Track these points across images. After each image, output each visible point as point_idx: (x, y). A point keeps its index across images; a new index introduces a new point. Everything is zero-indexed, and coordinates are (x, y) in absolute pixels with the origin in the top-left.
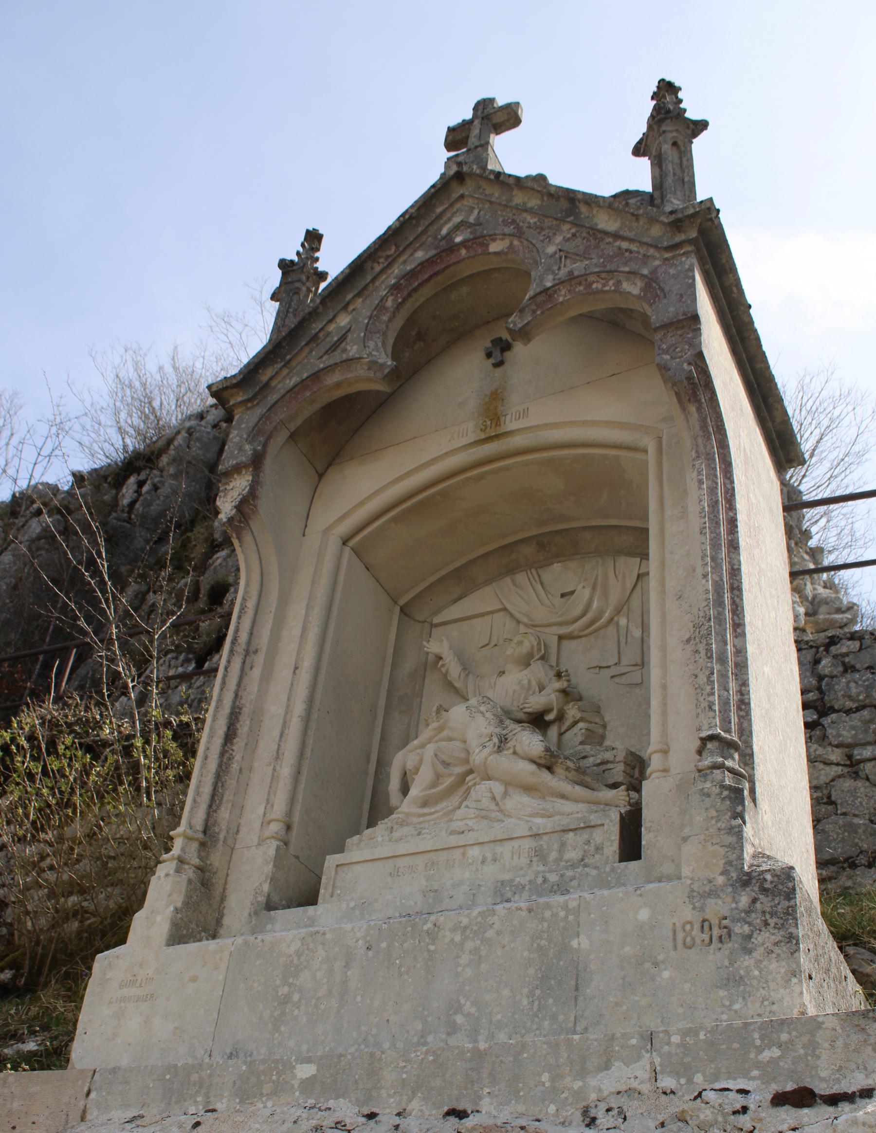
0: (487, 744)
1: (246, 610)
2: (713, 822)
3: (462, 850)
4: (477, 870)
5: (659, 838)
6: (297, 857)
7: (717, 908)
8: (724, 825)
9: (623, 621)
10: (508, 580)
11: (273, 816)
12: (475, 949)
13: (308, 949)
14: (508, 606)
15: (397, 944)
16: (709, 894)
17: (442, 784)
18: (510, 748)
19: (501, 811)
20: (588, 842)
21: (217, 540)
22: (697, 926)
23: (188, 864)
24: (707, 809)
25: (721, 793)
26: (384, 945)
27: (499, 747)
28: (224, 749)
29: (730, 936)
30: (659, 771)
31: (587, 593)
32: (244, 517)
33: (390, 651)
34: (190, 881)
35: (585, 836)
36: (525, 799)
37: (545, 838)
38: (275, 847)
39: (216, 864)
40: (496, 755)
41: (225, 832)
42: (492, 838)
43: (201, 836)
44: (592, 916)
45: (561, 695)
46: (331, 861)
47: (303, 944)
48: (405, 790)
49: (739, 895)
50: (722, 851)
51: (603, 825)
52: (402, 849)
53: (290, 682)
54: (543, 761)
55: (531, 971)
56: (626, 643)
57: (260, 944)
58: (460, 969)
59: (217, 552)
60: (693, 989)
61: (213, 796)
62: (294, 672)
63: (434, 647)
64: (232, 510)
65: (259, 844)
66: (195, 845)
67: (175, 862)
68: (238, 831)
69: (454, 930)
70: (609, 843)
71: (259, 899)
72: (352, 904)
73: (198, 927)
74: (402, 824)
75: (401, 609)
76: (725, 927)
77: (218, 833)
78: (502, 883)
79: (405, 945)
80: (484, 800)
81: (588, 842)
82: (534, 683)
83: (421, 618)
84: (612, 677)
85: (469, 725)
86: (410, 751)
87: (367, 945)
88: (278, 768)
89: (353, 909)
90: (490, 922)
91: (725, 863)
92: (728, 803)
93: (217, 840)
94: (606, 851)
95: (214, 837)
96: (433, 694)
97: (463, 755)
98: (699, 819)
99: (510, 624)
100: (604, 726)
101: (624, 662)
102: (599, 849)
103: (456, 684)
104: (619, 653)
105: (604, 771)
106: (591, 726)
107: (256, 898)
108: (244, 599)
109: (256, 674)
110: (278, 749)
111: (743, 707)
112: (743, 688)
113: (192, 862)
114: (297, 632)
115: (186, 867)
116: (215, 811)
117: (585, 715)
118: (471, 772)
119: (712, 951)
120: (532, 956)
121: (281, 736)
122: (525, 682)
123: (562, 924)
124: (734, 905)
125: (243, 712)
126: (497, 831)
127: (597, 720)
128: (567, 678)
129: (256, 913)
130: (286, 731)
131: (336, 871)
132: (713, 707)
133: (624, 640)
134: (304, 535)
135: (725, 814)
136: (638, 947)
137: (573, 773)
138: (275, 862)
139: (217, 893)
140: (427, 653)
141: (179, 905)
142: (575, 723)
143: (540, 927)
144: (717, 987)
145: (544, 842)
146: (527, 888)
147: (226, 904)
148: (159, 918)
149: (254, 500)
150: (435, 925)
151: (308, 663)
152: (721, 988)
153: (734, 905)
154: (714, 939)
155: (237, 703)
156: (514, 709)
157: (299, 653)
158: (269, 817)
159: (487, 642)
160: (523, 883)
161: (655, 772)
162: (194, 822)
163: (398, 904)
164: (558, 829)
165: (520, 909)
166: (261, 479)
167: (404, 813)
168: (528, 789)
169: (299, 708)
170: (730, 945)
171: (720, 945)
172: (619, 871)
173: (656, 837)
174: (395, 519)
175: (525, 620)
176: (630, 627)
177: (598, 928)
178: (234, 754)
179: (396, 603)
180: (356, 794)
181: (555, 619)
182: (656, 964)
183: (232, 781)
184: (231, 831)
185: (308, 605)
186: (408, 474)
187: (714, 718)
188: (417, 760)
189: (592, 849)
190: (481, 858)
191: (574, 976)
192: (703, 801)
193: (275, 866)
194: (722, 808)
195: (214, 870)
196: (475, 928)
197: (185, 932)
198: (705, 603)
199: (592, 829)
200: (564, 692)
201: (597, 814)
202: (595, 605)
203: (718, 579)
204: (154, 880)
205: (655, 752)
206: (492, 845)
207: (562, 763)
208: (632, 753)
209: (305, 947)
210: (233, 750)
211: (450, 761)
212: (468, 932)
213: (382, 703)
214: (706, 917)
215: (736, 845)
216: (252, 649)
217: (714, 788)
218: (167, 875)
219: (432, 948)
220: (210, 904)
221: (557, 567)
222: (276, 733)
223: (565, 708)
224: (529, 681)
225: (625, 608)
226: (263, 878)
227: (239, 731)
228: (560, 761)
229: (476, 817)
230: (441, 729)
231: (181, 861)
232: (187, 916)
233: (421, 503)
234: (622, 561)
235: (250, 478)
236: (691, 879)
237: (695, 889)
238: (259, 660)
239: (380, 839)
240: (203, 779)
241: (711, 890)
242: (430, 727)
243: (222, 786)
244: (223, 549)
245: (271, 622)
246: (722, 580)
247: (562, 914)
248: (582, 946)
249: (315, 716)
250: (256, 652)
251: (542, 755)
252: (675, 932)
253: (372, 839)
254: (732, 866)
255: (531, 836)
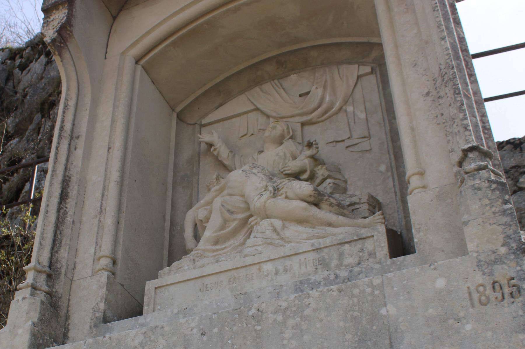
0: (264, 193)
1: (68, 107)
2: (488, 208)
3: (257, 266)
4: (272, 279)
5: (428, 236)
6: (122, 285)
7: (504, 272)
8: (497, 210)
9: (350, 109)
10: (257, 89)
11: (103, 254)
12: (297, 325)
13: (150, 341)
14: (259, 106)
15: (227, 329)
16: (495, 262)
17: (228, 227)
18: (282, 194)
19: (282, 239)
20: (362, 250)
21: (10, 132)
22: (489, 287)
23: (40, 290)
24: (480, 199)
25: (490, 186)
26: (216, 330)
27: (274, 194)
28: (60, 206)
29: (519, 292)
30: (419, 188)
31: (320, 92)
32: (63, 39)
33: (173, 144)
34: (42, 303)
35: (359, 245)
36: (300, 228)
37: (326, 250)
38: (107, 275)
39: (61, 291)
40: (273, 199)
41: (65, 267)
42: (282, 255)
43: (48, 269)
44: (395, 289)
45: (311, 160)
46: (150, 285)
47: (145, 337)
48: (197, 237)
49: (522, 260)
50: (500, 228)
51: (373, 236)
52: (208, 270)
53: (105, 158)
54: (312, 199)
55: (349, 336)
56: (355, 123)
57: (109, 341)
58: (285, 342)
59: (11, 140)
60: (495, 336)
61: (54, 241)
62: (108, 151)
63: (206, 137)
64: (54, 34)
65: (93, 275)
66: (44, 277)
67: (30, 288)
68: (74, 268)
69: (275, 312)
70: (380, 249)
71: (97, 315)
72: (176, 311)
73: (50, 338)
74: (202, 256)
75: (178, 116)
76: (514, 286)
77: (60, 268)
78: (301, 282)
79: (235, 328)
80: (267, 232)
81: (362, 250)
82: (288, 155)
83: (192, 122)
84: (347, 147)
85: (248, 183)
86: (198, 209)
87: (201, 332)
88: (102, 220)
89: (177, 314)
90: (307, 303)
91: (505, 237)
92: (498, 192)
93: (59, 274)
94: (378, 255)
95: (57, 271)
96: (208, 171)
97: (243, 205)
98: (475, 207)
99: (262, 119)
100: (345, 182)
101: (355, 135)
102: (371, 254)
103: (226, 163)
104: (350, 130)
105: (353, 210)
106: (337, 182)
107: (95, 314)
108: (66, 99)
109: (79, 152)
110: (101, 206)
111: (486, 132)
112: (484, 118)
113: (43, 289)
114: (107, 123)
115: (39, 292)
116: (57, 252)
117: (331, 174)
118: (251, 216)
119: (506, 305)
120: (347, 325)
121: (103, 196)
122: (282, 154)
123: (370, 298)
124: (518, 268)
125: (71, 180)
126: (282, 252)
127: (340, 177)
128: (316, 146)
129: (96, 326)
130: (106, 193)
131: (155, 292)
132: (468, 128)
133: (353, 121)
134: (105, 58)
135: (497, 201)
136: (440, 309)
137: (336, 207)
138: (107, 287)
139: (63, 313)
140: (200, 143)
141: (36, 320)
142: (324, 180)
143: (351, 302)
144: (517, 332)
145: (325, 253)
146: (322, 283)
147: (70, 321)
148: (20, 331)
149: (70, 27)
150: (258, 310)
151: (118, 144)
152: (520, 333)
153: (518, 268)
154: (506, 296)
155: (67, 173)
156: (276, 172)
157: (110, 137)
158: (98, 255)
159: (245, 133)
160: (318, 280)
161: (415, 189)
162: (41, 260)
163: (215, 306)
164: (335, 243)
165: (331, 290)
166: (74, 13)
167: (201, 250)
168: (301, 221)
169: (115, 175)
170: (521, 299)
171: (512, 300)
172: (399, 263)
173: (425, 235)
174: (174, 44)
175: (274, 114)
176: (356, 112)
177: (402, 298)
178: (67, 210)
179: (173, 110)
180: (159, 242)
181: (297, 112)
182: (458, 320)
183: (68, 230)
184: (69, 267)
185: (114, 104)
186: (183, 9)
187: (470, 135)
188: (210, 209)
189: (366, 255)
190: (274, 270)
191: (388, 337)
192: (476, 193)
193: (107, 290)
194: (493, 197)
195: (60, 296)
196: (294, 309)
197: (41, 341)
198: (447, 57)
199: (364, 241)
200: (313, 158)
201: (366, 229)
202: (327, 98)
203: (452, 41)
204: (13, 304)
205: (413, 175)
206: (282, 260)
207: (326, 200)
208: (372, 197)
209: (148, 339)
210: (66, 208)
211: (233, 210)
212: (288, 313)
213: (170, 179)
214: (496, 279)
215: (511, 223)
216: (75, 135)
217: (483, 183)
218: (24, 298)
219: (258, 328)
220: (58, 322)
221: (294, 77)
222: (99, 194)
223: (315, 169)
224: (285, 154)
225: (351, 99)
226: (99, 299)
227: (70, 194)
228: (325, 198)
229: (263, 244)
230: (221, 190)
231: (34, 288)
232: (42, 329)
233: (193, 30)
234: (344, 68)
235: (67, 11)
236: (477, 252)
237: (482, 259)
238: (81, 143)
239: (186, 268)
240: (46, 227)
241: (496, 259)
242: (212, 190)
243: (61, 234)
244: (14, 139)
245: (87, 117)
246: (456, 42)
247: (369, 290)
248: (390, 312)
249: (126, 182)
250: (78, 137)
251: (312, 193)
252: (470, 294)
253: (180, 268)
254: (511, 239)
255: (314, 250)
